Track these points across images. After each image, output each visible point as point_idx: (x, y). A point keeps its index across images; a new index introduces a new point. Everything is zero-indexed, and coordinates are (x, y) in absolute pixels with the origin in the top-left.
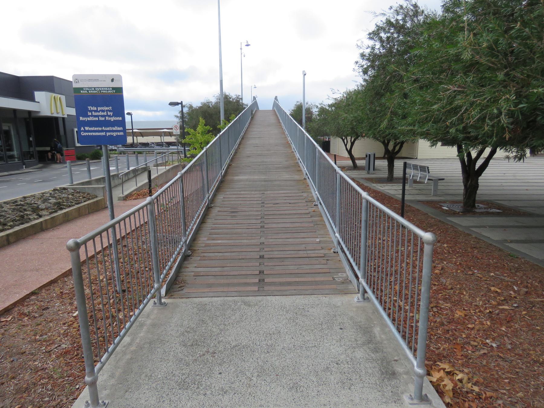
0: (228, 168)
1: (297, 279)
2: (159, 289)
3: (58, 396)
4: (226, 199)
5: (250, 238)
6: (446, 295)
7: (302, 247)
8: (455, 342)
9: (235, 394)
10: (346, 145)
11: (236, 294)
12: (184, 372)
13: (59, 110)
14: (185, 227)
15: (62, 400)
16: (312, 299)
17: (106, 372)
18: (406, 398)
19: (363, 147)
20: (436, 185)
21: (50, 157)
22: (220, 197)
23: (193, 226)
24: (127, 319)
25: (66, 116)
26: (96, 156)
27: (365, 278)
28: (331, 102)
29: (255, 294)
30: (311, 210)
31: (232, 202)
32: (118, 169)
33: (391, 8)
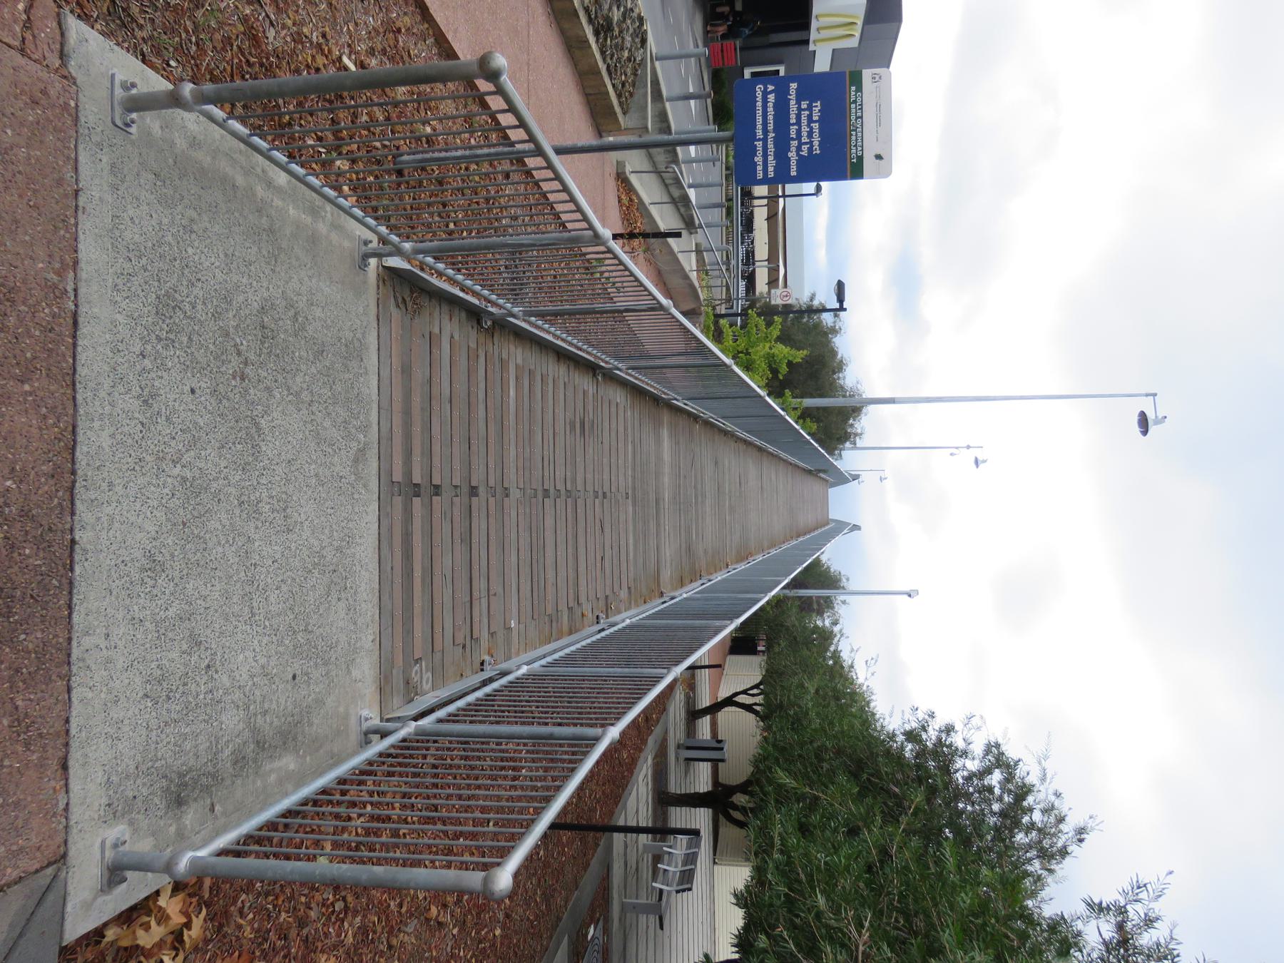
0: (689, 414)
1: (418, 574)
2: (398, 252)
3: (152, 20)
4: (613, 409)
5: (520, 465)
6: (375, 932)
7: (496, 587)
8: (258, 954)
9: (142, 424)
10: (745, 692)
11: (385, 430)
12: (199, 307)
13: (825, 34)
14: (570, 314)
15: (141, 27)
16: (369, 610)
17: (203, 130)
18: (118, 831)
19: (741, 732)
20: (647, 909)
21: (719, 10)
22: (619, 396)
23: (550, 332)
24: (333, 177)
25: (812, 47)
26: (721, 114)
27: (416, 734)
28: (845, 655)
29: (384, 474)
30: (587, 608)
31: (606, 424)
32: (690, 161)
33: (1058, 795)
